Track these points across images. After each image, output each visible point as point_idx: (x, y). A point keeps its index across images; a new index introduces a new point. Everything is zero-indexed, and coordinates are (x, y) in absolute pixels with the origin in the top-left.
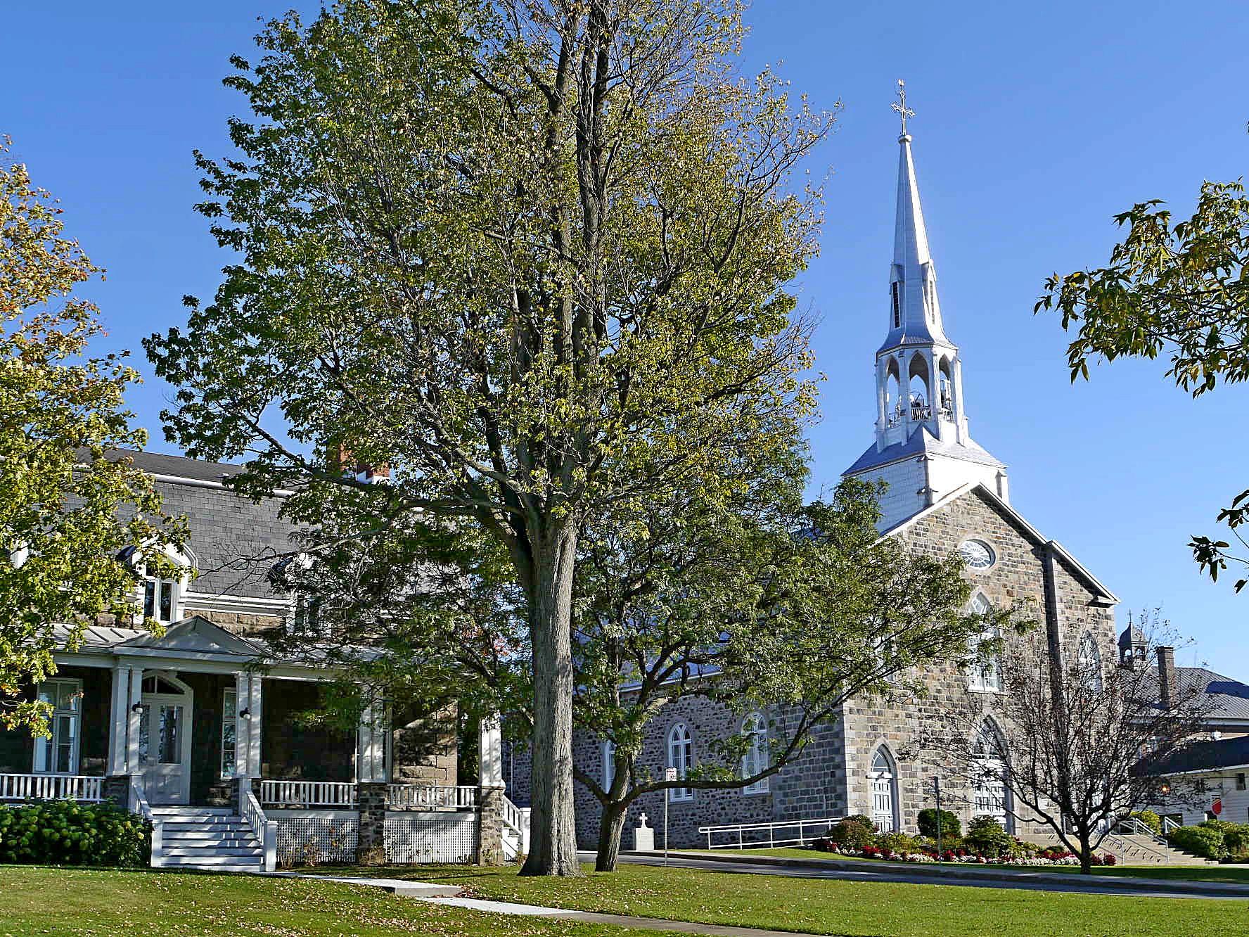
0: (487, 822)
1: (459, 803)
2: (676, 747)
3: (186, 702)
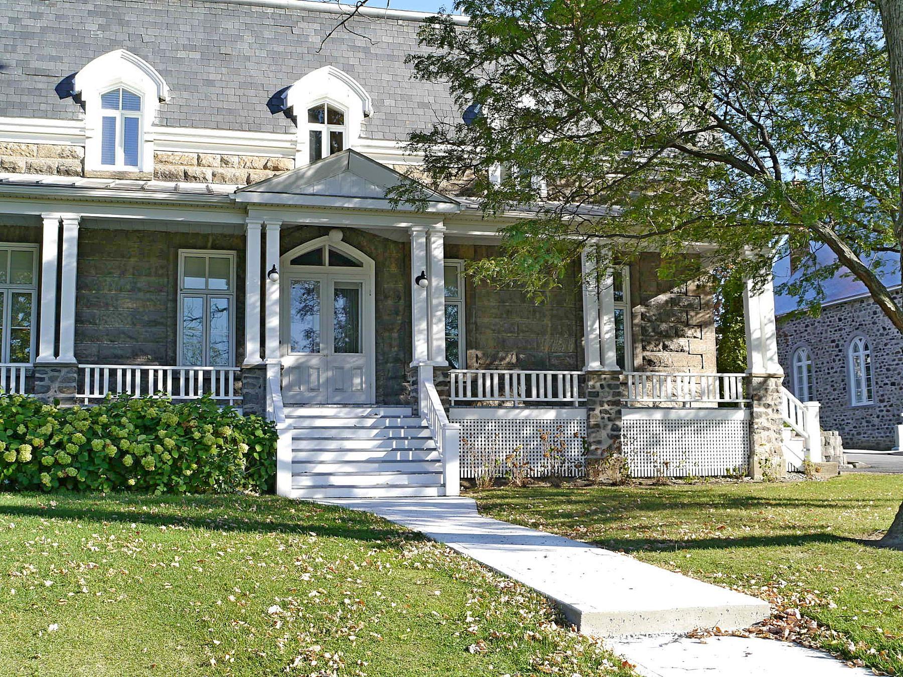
0: (760, 422)
1: (722, 396)
2: (800, 367)
3: (365, 275)
